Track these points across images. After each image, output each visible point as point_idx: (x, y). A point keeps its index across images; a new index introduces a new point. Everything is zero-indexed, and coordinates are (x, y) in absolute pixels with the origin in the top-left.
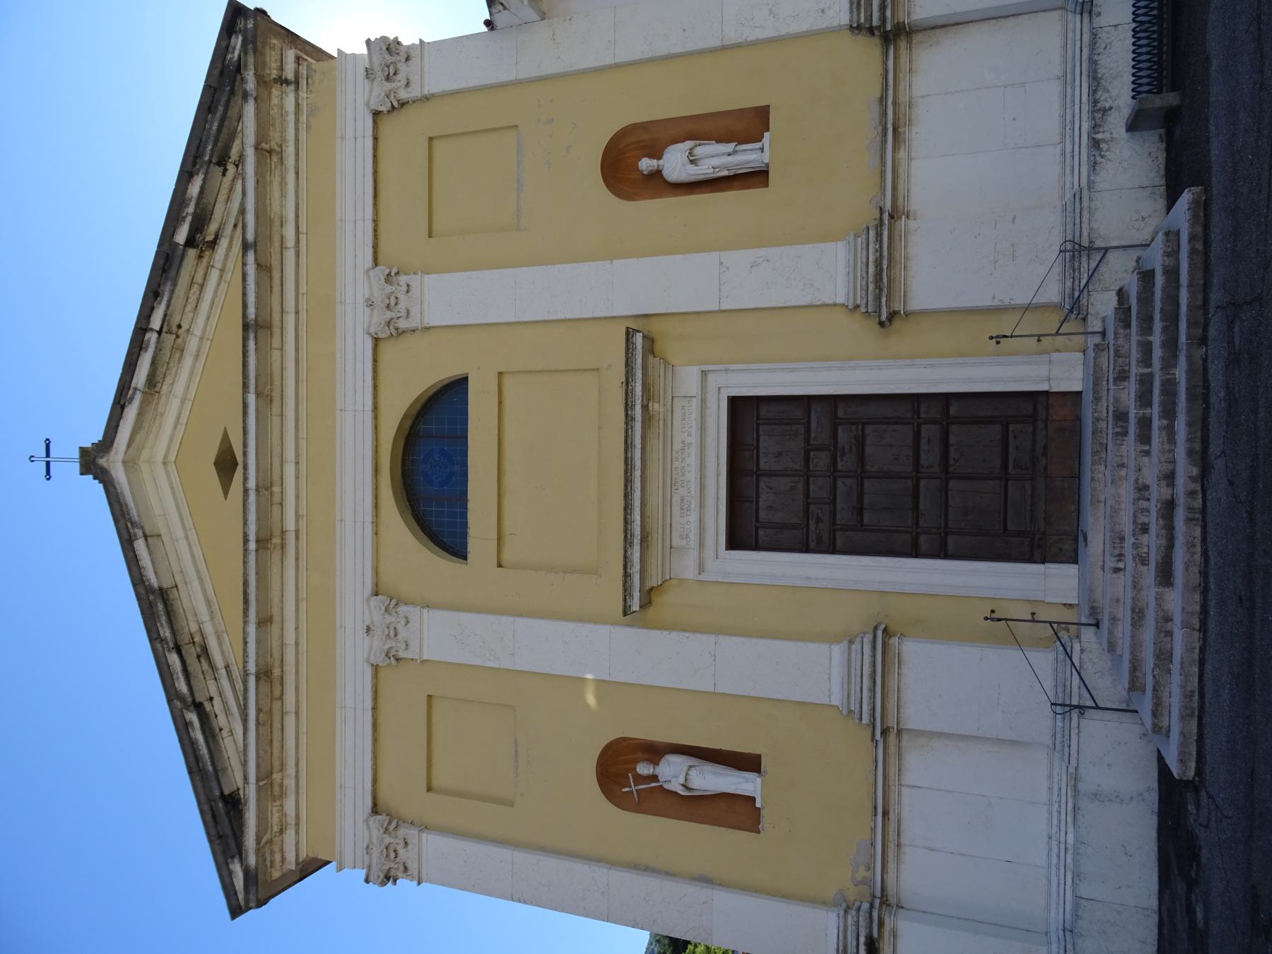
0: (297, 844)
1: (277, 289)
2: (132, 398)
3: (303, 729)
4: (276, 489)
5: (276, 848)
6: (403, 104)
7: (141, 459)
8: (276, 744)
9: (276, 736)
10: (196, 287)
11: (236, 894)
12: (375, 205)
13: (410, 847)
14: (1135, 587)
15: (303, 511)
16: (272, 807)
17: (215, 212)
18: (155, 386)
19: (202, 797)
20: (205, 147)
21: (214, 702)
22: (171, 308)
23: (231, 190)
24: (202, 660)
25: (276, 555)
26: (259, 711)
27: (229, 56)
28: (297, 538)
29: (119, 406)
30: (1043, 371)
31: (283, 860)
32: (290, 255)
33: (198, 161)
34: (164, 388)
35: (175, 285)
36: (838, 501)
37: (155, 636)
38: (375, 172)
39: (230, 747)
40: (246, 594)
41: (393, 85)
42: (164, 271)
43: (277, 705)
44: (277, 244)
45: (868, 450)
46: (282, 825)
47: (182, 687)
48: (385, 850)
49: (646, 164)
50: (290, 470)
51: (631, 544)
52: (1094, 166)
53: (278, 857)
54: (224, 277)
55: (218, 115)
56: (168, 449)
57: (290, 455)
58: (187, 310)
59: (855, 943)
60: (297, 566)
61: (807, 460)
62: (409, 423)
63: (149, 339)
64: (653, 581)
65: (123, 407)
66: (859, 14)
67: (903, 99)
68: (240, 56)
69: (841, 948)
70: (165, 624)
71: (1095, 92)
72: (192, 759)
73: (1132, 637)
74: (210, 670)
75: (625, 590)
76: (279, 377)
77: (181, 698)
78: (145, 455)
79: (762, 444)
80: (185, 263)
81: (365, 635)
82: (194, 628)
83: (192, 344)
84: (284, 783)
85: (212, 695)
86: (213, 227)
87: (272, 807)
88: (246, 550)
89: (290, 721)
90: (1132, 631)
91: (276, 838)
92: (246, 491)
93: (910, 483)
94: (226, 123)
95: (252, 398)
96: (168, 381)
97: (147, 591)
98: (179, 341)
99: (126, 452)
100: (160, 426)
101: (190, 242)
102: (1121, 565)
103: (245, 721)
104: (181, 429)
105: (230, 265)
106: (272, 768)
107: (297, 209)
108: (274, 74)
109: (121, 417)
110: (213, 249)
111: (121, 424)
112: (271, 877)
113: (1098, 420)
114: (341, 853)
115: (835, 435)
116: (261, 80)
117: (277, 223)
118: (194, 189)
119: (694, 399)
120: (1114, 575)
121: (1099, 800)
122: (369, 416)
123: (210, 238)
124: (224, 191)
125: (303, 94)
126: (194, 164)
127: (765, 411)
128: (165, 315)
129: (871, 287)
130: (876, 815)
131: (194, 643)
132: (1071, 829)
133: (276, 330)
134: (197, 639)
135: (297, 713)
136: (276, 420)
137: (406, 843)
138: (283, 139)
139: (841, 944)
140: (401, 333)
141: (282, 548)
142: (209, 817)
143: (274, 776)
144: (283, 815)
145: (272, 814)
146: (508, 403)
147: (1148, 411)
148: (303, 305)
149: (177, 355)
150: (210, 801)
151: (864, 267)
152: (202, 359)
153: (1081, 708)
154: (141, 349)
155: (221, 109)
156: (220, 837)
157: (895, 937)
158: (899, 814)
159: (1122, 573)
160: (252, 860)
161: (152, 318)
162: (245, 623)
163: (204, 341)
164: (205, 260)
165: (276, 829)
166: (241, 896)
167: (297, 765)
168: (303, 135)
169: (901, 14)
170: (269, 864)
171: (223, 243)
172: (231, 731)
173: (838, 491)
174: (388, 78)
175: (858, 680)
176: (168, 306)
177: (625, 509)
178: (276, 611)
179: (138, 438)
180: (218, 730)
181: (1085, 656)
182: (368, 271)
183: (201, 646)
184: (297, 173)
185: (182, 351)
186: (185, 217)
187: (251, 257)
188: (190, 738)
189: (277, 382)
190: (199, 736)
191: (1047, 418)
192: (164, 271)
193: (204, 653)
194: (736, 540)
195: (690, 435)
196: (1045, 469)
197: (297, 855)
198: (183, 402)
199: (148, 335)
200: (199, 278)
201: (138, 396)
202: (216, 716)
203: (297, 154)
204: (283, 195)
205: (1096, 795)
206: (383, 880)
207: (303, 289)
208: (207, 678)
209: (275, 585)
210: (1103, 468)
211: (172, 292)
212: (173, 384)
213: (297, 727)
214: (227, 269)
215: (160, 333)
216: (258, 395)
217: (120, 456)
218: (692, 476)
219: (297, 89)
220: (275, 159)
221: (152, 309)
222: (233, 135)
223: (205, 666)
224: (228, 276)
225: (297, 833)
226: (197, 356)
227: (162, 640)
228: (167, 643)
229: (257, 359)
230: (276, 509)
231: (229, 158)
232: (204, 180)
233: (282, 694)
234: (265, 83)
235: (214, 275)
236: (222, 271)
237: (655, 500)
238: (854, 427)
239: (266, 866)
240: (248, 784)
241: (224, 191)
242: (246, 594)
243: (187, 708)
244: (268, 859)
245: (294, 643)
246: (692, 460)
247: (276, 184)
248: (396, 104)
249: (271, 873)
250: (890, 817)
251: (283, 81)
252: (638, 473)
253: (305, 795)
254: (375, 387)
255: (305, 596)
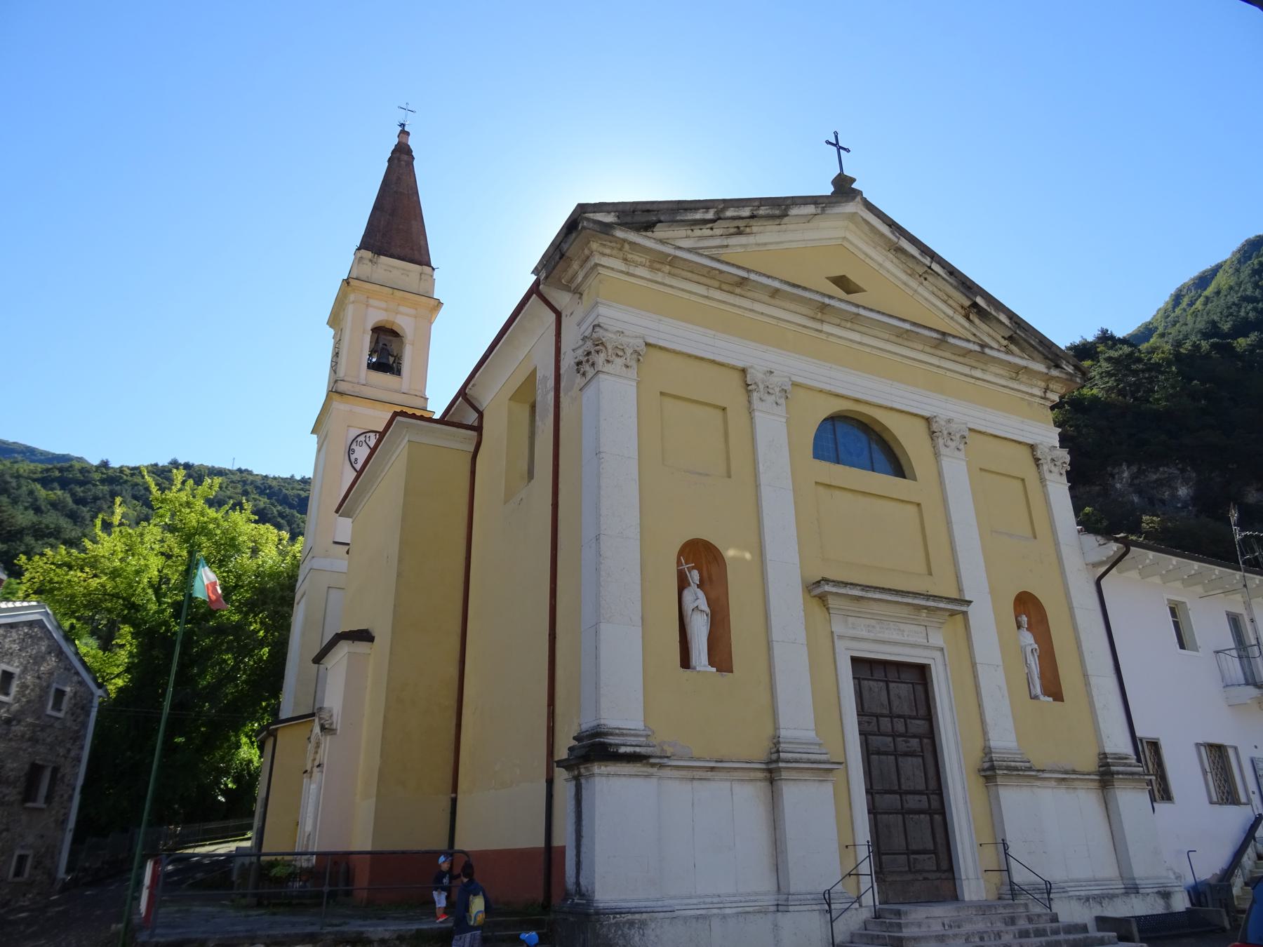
0: (613, 269)
1: (954, 357)
2: (893, 234)
3: (693, 298)
4: (849, 325)
5: (615, 252)
6: (749, 392)
7: (850, 224)
8: (689, 275)
9: (696, 277)
10: (946, 298)
11: (594, 212)
12: (992, 435)
13: (624, 369)
14: (954, 935)
15: (831, 339)
16: (646, 259)
17: (984, 324)
18: (895, 250)
19: (661, 206)
20: (1024, 333)
21: (709, 230)
22: (941, 279)
23: (994, 338)
24: (736, 230)
25: (811, 313)
26: (721, 272)
27: (1064, 362)
28: (817, 330)
29: (891, 223)
30: (971, 875)
31: (604, 255)
32: (966, 370)
33: (1017, 326)
34: (891, 256)
35: (955, 287)
36: (880, 738)
37: (763, 203)
38: (1005, 439)
39: (681, 232)
40: (799, 287)
41: (1049, 462)
42: (963, 283)
43: (716, 284)
44: (974, 364)
45: (910, 759)
46: (630, 261)
47: (730, 213)
48: (622, 348)
49: (695, 576)
50: (856, 337)
51: (863, 590)
52: (1079, 898)
53: (608, 251)
54: (947, 318)
55: (1038, 346)
56: (851, 243)
57: (866, 340)
58: (934, 288)
59: (633, 743)
60: (800, 325)
61: (899, 716)
62: (877, 429)
63: (927, 259)
64: (832, 602)
65: (890, 226)
66: (1111, 759)
67: (1076, 784)
68: (1064, 369)
69: (625, 732)
70: (767, 212)
71: (1107, 897)
72: (686, 206)
73: (930, 936)
74: (728, 233)
75: (838, 582)
76: (908, 345)
77: (723, 210)
78: (852, 226)
79: (903, 685)
80: (964, 298)
81: (765, 369)
82: (755, 229)
83: (913, 284)
84: (660, 273)
85: (715, 230)
86: (977, 321)
87: (646, 259)
88: (824, 295)
89: (701, 290)
90: (933, 936)
91: (622, 255)
92: (830, 297)
93: (896, 788)
94: (1032, 349)
95: (907, 326)
96: (895, 260)
97: (787, 205)
98: (917, 276)
99: (862, 217)
100: (867, 243)
101: (975, 305)
102: (947, 927)
103: (689, 250)
104: (863, 257)
105: (953, 324)
106: (674, 267)
107: (988, 382)
108: (1051, 386)
109: (884, 222)
110: (964, 316)
111: (879, 220)
112: (593, 241)
113: (996, 908)
114: (610, 306)
115: (914, 736)
116: (1052, 378)
117: (985, 368)
118: (1003, 318)
119: (926, 641)
120: (941, 924)
121: (773, 929)
122: (889, 404)
123: (971, 317)
124: (994, 334)
125: (1038, 400)
126: (1016, 323)
127: (920, 688)
128: (939, 275)
129: (1005, 763)
130: (716, 761)
131: (746, 226)
132: (734, 910)
133: (932, 351)
134: (748, 230)
135: (707, 297)
136: (886, 336)
137: (628, 367)
138: (1021, 382)
139: (628, 732)
140: (749, 392)
141: (813, 318)
142: (648, 207)
143: (668, 267)
144: (637, 265)
145: (641, 257)
146: (901, 505)
147: (1032, 935)
148: (941, 372)
149: (909, 272)
150: (658, 211)
151: (1012, 759)
152: (903, 287)
153: (830, 911)
154: (922, 251)
155: (1041, 349)
156: (634, 212)
157: (647, 776)
158: (714, 780)
159: (943, 928)
160: (620, 234)
161: (938, 265)
162: (781, 281)
163: (913, 292)
164: (959, 309)
165: (629, 256)
166: (591, 215)
167: (739, 307)
168: (1019, 395)
169: (1118, 783)
170: (604, 243)
171: (966, 324)
172: (689, 237)
173: (886, 738)
174: (1053, 460)
175: (805, 751)
176: (943, 279)
177: (883, 589)
178: (777, 302)
179: (866, 228)
180: (692, 228)
181: (854, 911)
182: (643, 338)
183: (743, 231)
184: (1004, 386)
185: (910, 275)
186: (989, 307)
187: (977, 348)
188: (699, 209)
189: (906, 343)
190: (699, 216)
191: (942, 879)
192: (963, 283)
193: (739, 232)
194: (922, 672)
195: (908, 636)
196: (917, 880)
197: (604, 266)
198: (880, 265)
199: (929, 259)
200: (950, 302)
201: (895, 239)
202: (701, 229)
203: (1013, 389)
204: (996, 375)
205: (776, 926)
206: (601, 339)
207: (948, 374)
208: (725, 230)
209: (793, 306)
210: (974, 913)
211: (951, 284)
212: (892, 262)
213: (696, 294)
214: (952, 321)
215: (930, 268)
216: (908, 331)
217: (860, 212)
218: (886, 635)
219: (1041, 398)
220: (1014, 375)
221: (944, 268)
222: (1022, 350)
223: (732, 230)
224: (947, 320)
225: (622, 272)
226: (905, 284)
227: (759, 207)
228: (756, 210)
229: (927, 337)
230: (838, 321)
231: (1011, 343)
232: (1007, 326)
233: (721, 290)
234: (1048, 380)
235: (950, 312)
236: (952, 318)
237: (876, 608)
238: (920, 750)
239: (606, 241)
240: (675, 248)
241: (994, 334)
242: (799, 287)
243: (716, 213)
244: (609, 244)
245: (754, 309)
246: (895, 637)
247: (1002, 372)
248: (750, 388)
249: (597, 242)
250: (709, 773)
251: (1046, 390)
252: (899, 599)
253: (645, 285)
254: (690, 356)
255: (779, 325)
